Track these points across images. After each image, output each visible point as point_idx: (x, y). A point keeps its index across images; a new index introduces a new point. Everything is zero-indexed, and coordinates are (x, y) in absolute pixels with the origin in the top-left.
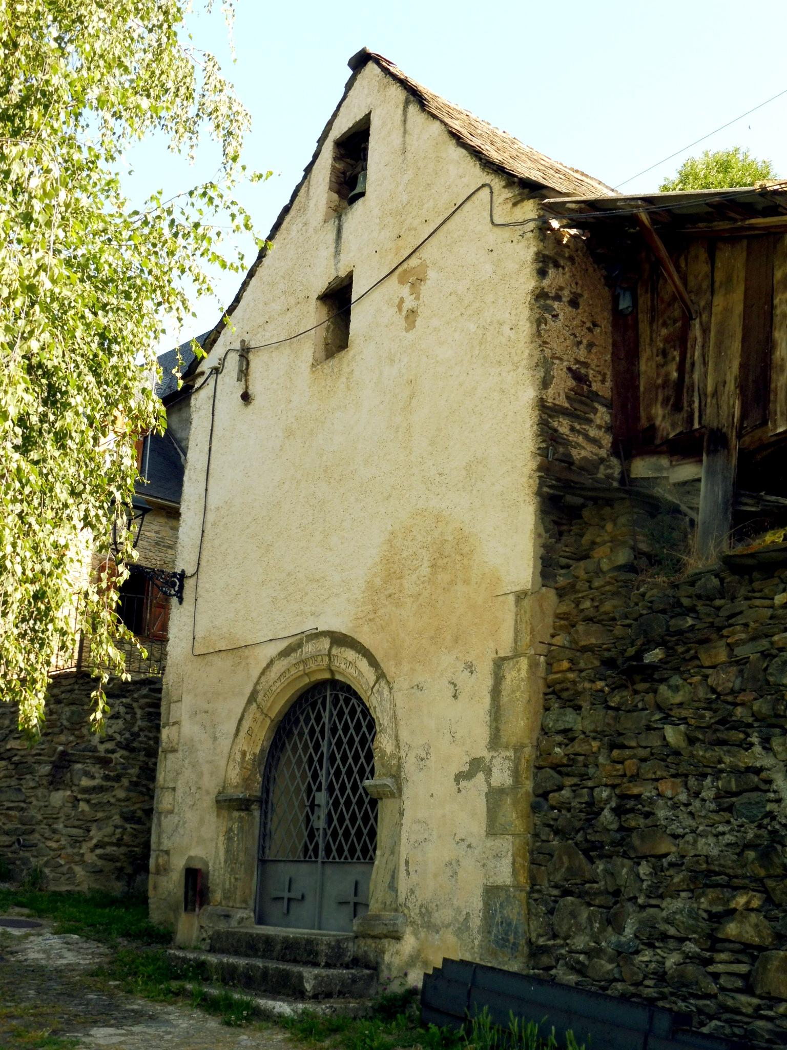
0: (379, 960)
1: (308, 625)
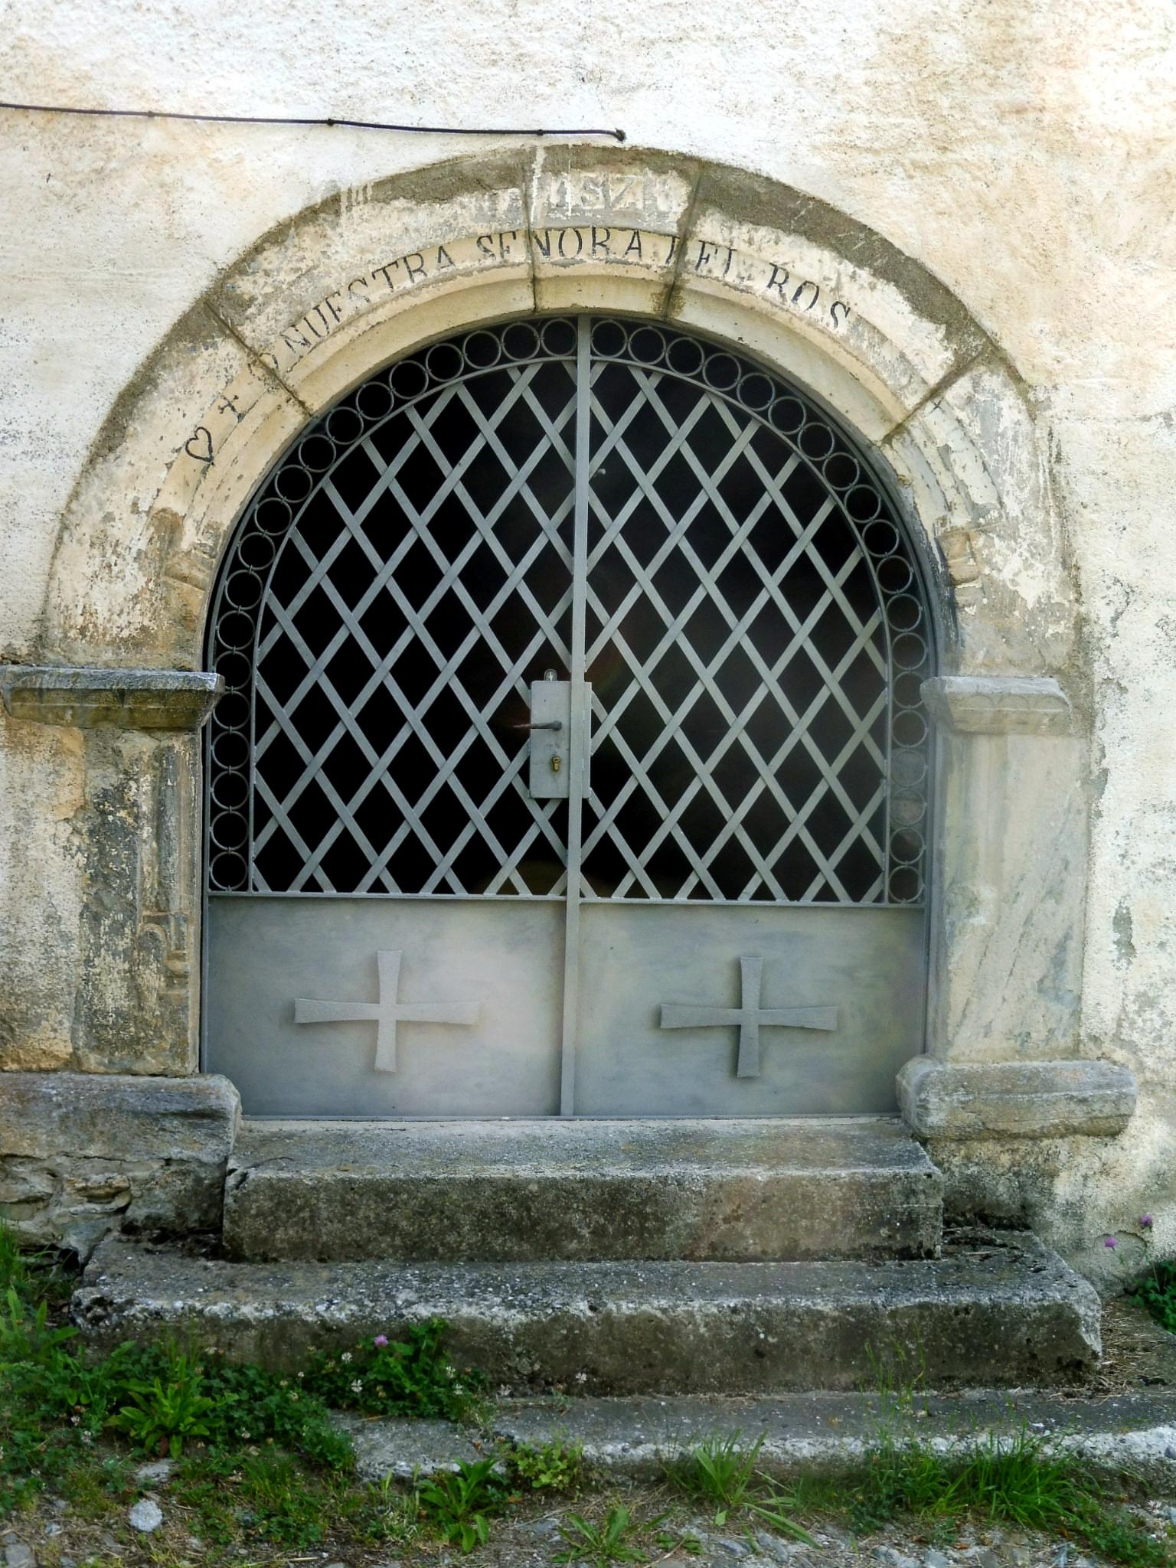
0: (1033, 1196)
1: (577, 112)
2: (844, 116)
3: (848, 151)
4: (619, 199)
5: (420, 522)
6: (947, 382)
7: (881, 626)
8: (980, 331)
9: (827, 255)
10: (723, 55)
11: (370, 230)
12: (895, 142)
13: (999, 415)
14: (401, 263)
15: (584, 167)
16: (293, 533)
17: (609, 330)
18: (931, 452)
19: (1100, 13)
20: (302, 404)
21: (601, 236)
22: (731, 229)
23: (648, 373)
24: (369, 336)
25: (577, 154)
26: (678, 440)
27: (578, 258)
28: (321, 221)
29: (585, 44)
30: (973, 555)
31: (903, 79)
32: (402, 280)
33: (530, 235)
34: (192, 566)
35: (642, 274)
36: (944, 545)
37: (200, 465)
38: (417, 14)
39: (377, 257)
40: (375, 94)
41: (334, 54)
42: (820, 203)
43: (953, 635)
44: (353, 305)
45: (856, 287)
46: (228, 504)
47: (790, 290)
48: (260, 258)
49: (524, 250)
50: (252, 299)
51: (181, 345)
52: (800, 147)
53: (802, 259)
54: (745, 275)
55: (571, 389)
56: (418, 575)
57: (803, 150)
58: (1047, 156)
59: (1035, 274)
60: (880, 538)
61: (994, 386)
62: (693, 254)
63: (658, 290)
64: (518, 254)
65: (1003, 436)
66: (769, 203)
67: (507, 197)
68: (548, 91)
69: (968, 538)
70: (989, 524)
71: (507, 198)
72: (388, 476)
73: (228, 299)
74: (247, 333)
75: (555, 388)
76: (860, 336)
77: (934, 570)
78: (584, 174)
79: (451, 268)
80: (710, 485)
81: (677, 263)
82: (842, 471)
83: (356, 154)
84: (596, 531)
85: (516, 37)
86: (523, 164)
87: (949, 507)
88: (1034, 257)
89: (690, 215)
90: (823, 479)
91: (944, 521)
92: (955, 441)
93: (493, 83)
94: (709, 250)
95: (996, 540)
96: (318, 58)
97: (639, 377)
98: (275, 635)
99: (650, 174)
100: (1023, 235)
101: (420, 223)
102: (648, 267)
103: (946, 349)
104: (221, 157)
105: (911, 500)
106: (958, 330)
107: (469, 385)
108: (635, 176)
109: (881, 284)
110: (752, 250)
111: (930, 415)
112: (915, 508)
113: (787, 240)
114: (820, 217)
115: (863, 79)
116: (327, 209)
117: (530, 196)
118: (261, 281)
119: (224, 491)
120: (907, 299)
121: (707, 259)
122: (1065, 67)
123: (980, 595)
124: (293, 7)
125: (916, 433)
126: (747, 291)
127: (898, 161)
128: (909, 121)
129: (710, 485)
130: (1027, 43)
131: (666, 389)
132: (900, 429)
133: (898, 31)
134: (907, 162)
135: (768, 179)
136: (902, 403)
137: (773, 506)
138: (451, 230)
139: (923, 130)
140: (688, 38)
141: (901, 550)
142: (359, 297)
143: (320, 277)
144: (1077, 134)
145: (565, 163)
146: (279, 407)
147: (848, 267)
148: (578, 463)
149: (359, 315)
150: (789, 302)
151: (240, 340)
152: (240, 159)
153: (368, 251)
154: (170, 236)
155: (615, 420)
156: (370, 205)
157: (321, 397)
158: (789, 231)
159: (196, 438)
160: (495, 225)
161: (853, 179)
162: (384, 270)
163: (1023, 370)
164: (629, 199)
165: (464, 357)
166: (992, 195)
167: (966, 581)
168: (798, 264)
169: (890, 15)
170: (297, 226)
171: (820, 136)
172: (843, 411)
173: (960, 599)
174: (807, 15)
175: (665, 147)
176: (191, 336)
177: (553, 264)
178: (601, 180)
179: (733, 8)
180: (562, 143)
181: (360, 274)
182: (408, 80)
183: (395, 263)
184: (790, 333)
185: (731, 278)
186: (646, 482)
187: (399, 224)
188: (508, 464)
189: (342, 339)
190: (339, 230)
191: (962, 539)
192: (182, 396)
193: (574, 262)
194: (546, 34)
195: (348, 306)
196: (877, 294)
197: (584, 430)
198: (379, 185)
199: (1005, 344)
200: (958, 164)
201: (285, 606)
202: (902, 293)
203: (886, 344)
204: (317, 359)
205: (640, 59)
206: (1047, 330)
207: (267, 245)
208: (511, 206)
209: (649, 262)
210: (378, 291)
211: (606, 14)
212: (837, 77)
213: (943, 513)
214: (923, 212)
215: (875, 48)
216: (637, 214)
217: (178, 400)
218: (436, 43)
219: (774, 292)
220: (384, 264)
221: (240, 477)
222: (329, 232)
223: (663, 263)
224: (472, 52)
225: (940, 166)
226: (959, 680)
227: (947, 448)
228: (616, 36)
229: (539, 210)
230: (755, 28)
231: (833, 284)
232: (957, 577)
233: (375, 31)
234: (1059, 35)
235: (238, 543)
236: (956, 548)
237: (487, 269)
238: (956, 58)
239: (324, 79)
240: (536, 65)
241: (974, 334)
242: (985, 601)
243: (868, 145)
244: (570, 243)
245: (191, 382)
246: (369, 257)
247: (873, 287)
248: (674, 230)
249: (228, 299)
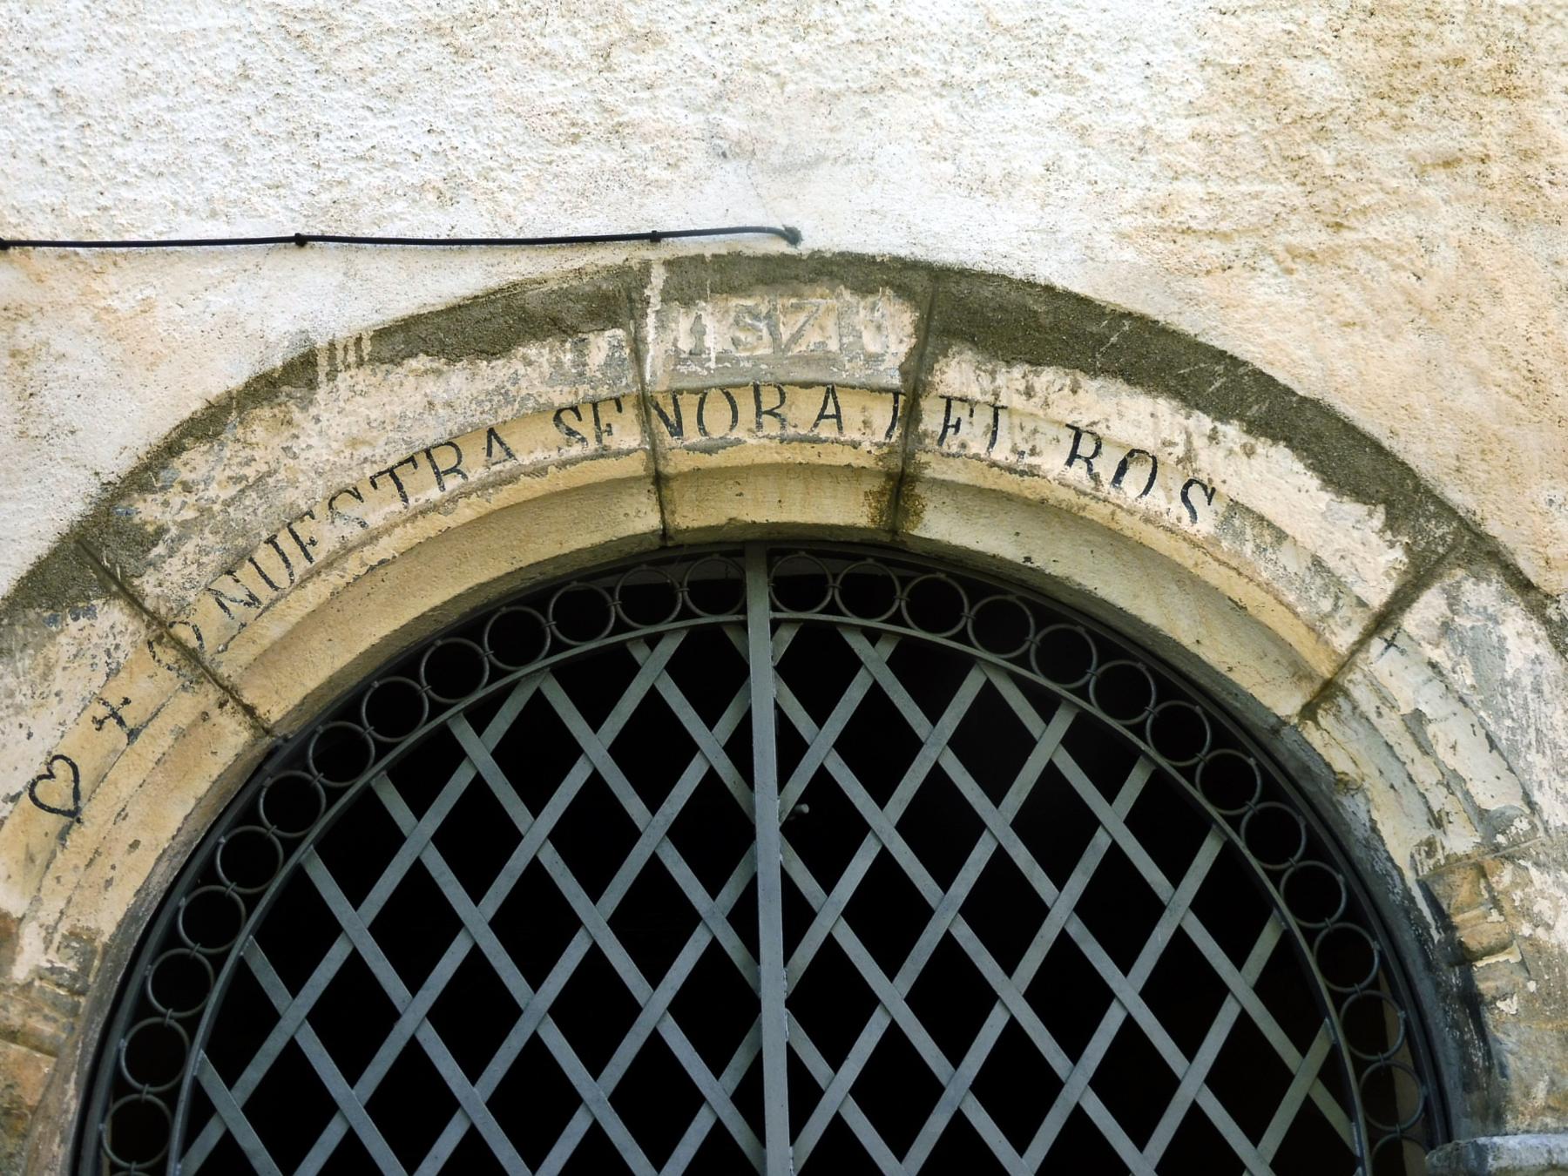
1: (710, 203)
2: (1163, 188)
3: (1179, 239)
4: (796, 337)
5: (476, 919)
6: (1402, 600)
7: (1334, 1052)
8: (1446, 510)
9: (1164, 405)
10: (954, 108)
11: (365, 409)
12: (1254, 220)
13: (1501, 648)
14: (422, 460)
15: (734, 290)
16: (245, 945)
17: (803, 563)
18: (1391, 727)
19: (1546, 22)
20: (249, 710)
21: (770, 399)
22: (993, 373)
23: (873, 636)
24: (366, 586)
25: (721, 270)
26: (935, 745)
27: (733, 436)
28: (283, 398)
29: (725, 103)
30: (1496, 903)
31: (1253, 128)
32: (423, 488)
33: (645, 403)
34: (31, 1010)
35: (845, 457)
36: (1438, 890)
37: (53, 822)
38: (448, 76)
39: (379, 452)
40: (376, 194)
41: (311, 141)
42: (1142, 321)
43: (1478, 1057)
44: (337, 533)
45: (1221, 454)
46: (112, 893)
47: (1106, 466)
48: (177, 463)
49: (637, 429)
50: (161, 531)
51: (32, 614)
52: (1097, 237)
53: (1121, 415)
54: (1026, 448)
55: (738, 672)
56: (475, 1014)
57: (1103, 240)
58: (1506, 228)
59: (1521, 410)
60: (1313, 895)
61: (1484, 601)
62: (932, 421)
63: (876, 484)
64: (627, 434)
65: (1514, 685)
66: (1055, 328)
67: (602, 345)
68: (666, 175)
69: (1482, 873)
70: (1514, 843)
71: (604, 345)
72: (419, 837)
73: (119, 533)
74: (148, 589)
75: (713, 673)
76: (1239, 535)
77: (1423, 940)
78: (735, 302)
79: (508, 465)
80: (998, 823)
81: (905, 436)
82: (1229, 782)
83: (342, 287)
84: (798, 915)
85: (609, 99)
86: (629, 291)
87: (1437, 821)
88: (1514, 382)
89: (921, 357)
90: (1198, 795)
91: (1430, 847)
92: (1430, 701)
93: (573, 168)
94: (959, 411)
95: (1534, 872)
96: (284, 149)
97: (858, 644)
98: (210, 1136)
99: (847, 295)
100: (1491, 350)
101: (452, 392)
102: (855, 445)
103: (1392, 545)
104: (116, 304)
105: (1363, 817)
106: (1407, 511)
107: (562, 673)
108: (821, 300)
109: (1262, 446)
110: (1031, 406)
111: (1380, 661)
112: (1374, 829)
113: (1090, 385)
114: (1145, 343)
115: (1189, 131)
116: (296, 376)
117: (644, 341)
118: (176, 501)
119: (101, 870)
120: (1310, 467)
121: (957, 427)
122: (1508, 96)
123: (1520, 977)
124: (247, 77)
125: (1361, 694)
126: (1032, 472)
127: (1263, 249)
128: (1271, 188)
129: (998, 823)
130: (1442, 67)
131: (908, 662)
132: (1328, 692)
133: (1234, 61)
134: (1279, 249)
135: (1049, 289)
136: (1327, 643)
137: (1115, 850)
138: (508, 399)
139: (1299, 201)
140: (894, 86)
141: (1354, 912)
142: (347, 520)
143: (278, 489)
144: (1548, 190)
145: (702, 286)
146: (205, 716)
147: (1203, 422)
148: (758, 798)
149: (347, 549)
150: (1107, 486)
151: (135, 602)
152: (147, 307)
153: (364, 442)
154: (23, 434)
155: (820, 719)
156: (367, 369)
157: (283, 697)
158: (1094, 372)
159: (51, 776)
160: (584, 390)
161: (1193, 281)
162: (391, 471)
163: (1530, 568)
164: (813, 338)
165: (550, 626)
166: (1429, 292)
167: (1490, 952)
168: (1115, 423)
169: (1216, 39)
170: (241, 408)
171: (1129, 218)
172: (1223, 669)
173: (1485, 986)
174: (1082, 45)
175: (870, 249)
176: (49, 596)
177: (688, 449)
178: (764, 309)
179: (965, 41)
180: (692, 253)
181: (348, 481)
182: (433, 172)
183: (411, 459)
184: (1115, 541)
185: (1001, 453)
186: (883, 823)
187: (418, 397)
188: (634, 805)
189: (317, 592)
190: (313, 411)
191: (1471, 874)
192: (28, 702)
193: (724, 444)
194: (661, 93)
195: (327, 535)
196: (1258, 462)
197: (768, 739)
198: (382, 334)
199: (1492, 528)
200: (1365, 248)
201: (230, 1082)
202: (1301, 459)
203: (1287, 544)
204: (272, 629)
205: (817, 121)
206: (1559, 499)
207: (188, 442)
208: (610, 357)
209: (857, 436)
210: (381, 508)
211: (757, 60)
212: (1145, 130)
213: (1426, 833)
214: (1317, 324)
215: (1199, 86)
216: (829, 360)
217: (19, 709)
218: (478, 114)
219: (1078, 472)
220: (392, 462)
221: (135, 845)
222: (297, 415)
223: (880, 437)
224: (537, 123)
225: (1335, 252)
226: (1512, 1142)
227: (1418, 715)
228: (774, 90)
229: (659, 362)
230: (1004, 68)
231: (1179, 451)
232: (1473, 945)
233: (378, 104)
234: (1489, 52)
235: (146, 969)
236: (1464, 893)
237: (573, 462)
238: (1333, 92)
239: (293, 177)
240: (645, 138)
241: (1436, 516)
242: (1532, 986)
243: (1211, 226)
244: (717, 417)
245: (45, 677)
246: (366, 451)
247: (1250, 452)
248: (896, 381)
249: (119, 533)
